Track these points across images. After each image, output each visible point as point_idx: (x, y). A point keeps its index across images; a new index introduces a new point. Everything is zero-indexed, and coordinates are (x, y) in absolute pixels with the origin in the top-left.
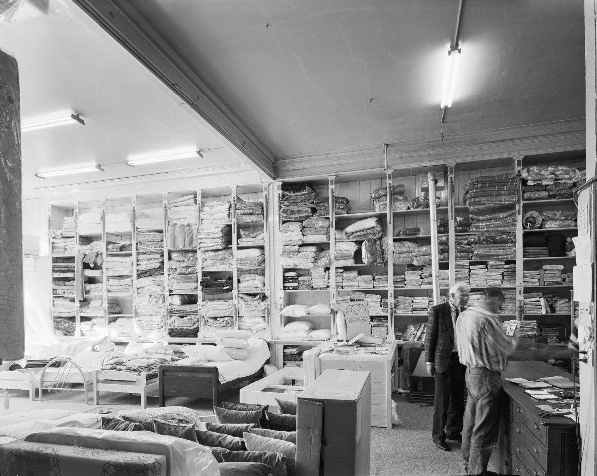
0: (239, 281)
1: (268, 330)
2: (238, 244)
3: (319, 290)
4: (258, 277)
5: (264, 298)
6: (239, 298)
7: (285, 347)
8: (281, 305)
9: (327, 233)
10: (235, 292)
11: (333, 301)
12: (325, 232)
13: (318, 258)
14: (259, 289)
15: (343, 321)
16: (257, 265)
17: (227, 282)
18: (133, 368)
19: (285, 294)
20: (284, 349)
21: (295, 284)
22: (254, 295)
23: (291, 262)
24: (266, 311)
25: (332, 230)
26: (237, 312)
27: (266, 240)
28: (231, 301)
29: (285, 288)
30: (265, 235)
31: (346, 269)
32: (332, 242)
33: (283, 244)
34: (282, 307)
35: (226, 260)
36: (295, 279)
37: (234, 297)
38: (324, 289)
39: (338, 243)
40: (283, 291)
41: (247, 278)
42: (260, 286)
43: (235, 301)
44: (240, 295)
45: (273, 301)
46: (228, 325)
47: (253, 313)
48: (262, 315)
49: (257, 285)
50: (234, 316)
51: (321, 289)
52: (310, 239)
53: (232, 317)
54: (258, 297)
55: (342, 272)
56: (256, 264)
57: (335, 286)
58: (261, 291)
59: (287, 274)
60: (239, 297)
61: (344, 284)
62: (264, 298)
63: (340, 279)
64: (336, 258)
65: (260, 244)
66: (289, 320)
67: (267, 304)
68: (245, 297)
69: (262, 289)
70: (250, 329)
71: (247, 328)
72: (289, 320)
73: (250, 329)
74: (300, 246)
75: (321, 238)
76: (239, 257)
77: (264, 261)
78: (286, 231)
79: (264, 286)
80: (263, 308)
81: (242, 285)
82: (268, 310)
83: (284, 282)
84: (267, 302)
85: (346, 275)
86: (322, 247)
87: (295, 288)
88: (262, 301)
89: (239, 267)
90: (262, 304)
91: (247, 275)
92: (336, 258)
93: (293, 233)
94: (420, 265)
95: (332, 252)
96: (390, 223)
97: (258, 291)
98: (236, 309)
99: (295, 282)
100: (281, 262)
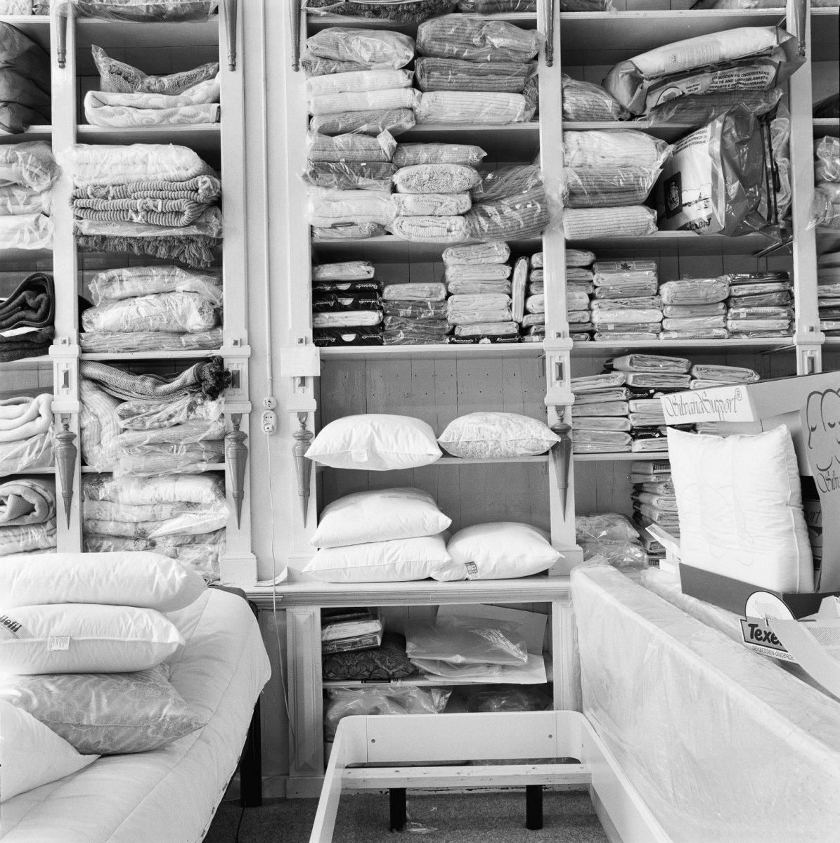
0: (84, 304)
1: (238, 542)
2: (81, 118)
3: (485, 345)
4: (184, 281)
5: (218, 381)
6: (86, 385)
7: (330, 616)
8: (302, 416)
9: (528, 87)
10: (62, 355)
11: (559, 392)
12: (521, 80)
13: (489, 194)
14: (194, 339)
15: (793, 489)
16: (184, 219)
17: (24, 305)
18: (82, 798)
19: (324, 360)
20: (324, 624)
21: (369, 318)
22: (162, 369)
23: (360, 210)
24: (229, 449)
25: (550, 77)
26: (75, 451)
27: (231, 104)
28: (43, 398)
29: (322, 336)
30: (225, 80)
31: (607, 252)
32: (548, 129)
33: (315, 124)
34: (311, 427)
35: (18, 193)
36: (371, 293)
37: (58, 381)
38: (508, 338)
39: (573, 137)
40: (316, 350)
41: (128, 288)
42: (196, 321)
43: (66, 400)
44: (92, 371)
45: (263, 399)
46: (28, 519)
47: (161, 459)
48: (204, 467)
49: (184, 318)
50: (58, 471)
51: (494, 339)
52: (450, 107)
53: (50, 478)
54: (188, 375)
55: (589, 268)
56: (178, 213)
57: (566, 328)
58: (203, 346)
59: (329, 272)
60: (83, 377)
61: (599, 317)
62: (218, 381)
63: (581, 297)
64: (574, 199)
65: (202, 123)
66: (332, 486)
67: (237, 409)
68: (119, 379)
69: (208, 337)
70: (141, 536)
71: (129, 530)
72: (332, 486)
73: (141, 536)
74: (404, 138)
75: (496, 109)
76: (86, 183)
77: (217, 203)
78: (330, 63)
79: (219, 322)
80: (214, 430)
81: (102, 318)
82: (240, 439)
83: (316, 310)
84: (235, 401)
85: (606, 278)
86: (507, 152)
87: (365, 335)
88: (213, 394)
89: (86, 227)
90: (211, 409)
91: (126, 272)
92: (574, 199)
93: (366, 75)
94: (829, 255)
95: (553, 170)
96: (62, 63)
97: (189, 347)
98: (68, 439)
99: (367, 307)
100: (310, 207)
